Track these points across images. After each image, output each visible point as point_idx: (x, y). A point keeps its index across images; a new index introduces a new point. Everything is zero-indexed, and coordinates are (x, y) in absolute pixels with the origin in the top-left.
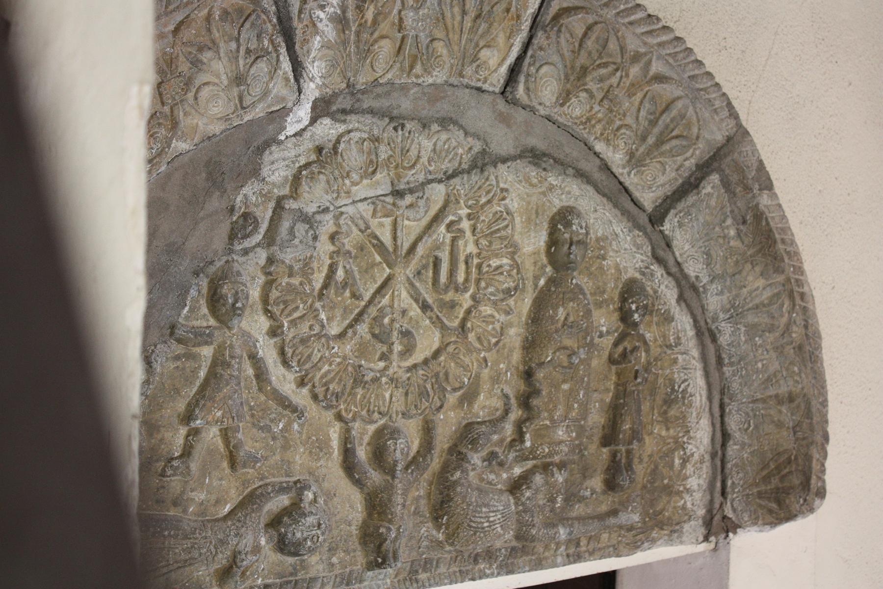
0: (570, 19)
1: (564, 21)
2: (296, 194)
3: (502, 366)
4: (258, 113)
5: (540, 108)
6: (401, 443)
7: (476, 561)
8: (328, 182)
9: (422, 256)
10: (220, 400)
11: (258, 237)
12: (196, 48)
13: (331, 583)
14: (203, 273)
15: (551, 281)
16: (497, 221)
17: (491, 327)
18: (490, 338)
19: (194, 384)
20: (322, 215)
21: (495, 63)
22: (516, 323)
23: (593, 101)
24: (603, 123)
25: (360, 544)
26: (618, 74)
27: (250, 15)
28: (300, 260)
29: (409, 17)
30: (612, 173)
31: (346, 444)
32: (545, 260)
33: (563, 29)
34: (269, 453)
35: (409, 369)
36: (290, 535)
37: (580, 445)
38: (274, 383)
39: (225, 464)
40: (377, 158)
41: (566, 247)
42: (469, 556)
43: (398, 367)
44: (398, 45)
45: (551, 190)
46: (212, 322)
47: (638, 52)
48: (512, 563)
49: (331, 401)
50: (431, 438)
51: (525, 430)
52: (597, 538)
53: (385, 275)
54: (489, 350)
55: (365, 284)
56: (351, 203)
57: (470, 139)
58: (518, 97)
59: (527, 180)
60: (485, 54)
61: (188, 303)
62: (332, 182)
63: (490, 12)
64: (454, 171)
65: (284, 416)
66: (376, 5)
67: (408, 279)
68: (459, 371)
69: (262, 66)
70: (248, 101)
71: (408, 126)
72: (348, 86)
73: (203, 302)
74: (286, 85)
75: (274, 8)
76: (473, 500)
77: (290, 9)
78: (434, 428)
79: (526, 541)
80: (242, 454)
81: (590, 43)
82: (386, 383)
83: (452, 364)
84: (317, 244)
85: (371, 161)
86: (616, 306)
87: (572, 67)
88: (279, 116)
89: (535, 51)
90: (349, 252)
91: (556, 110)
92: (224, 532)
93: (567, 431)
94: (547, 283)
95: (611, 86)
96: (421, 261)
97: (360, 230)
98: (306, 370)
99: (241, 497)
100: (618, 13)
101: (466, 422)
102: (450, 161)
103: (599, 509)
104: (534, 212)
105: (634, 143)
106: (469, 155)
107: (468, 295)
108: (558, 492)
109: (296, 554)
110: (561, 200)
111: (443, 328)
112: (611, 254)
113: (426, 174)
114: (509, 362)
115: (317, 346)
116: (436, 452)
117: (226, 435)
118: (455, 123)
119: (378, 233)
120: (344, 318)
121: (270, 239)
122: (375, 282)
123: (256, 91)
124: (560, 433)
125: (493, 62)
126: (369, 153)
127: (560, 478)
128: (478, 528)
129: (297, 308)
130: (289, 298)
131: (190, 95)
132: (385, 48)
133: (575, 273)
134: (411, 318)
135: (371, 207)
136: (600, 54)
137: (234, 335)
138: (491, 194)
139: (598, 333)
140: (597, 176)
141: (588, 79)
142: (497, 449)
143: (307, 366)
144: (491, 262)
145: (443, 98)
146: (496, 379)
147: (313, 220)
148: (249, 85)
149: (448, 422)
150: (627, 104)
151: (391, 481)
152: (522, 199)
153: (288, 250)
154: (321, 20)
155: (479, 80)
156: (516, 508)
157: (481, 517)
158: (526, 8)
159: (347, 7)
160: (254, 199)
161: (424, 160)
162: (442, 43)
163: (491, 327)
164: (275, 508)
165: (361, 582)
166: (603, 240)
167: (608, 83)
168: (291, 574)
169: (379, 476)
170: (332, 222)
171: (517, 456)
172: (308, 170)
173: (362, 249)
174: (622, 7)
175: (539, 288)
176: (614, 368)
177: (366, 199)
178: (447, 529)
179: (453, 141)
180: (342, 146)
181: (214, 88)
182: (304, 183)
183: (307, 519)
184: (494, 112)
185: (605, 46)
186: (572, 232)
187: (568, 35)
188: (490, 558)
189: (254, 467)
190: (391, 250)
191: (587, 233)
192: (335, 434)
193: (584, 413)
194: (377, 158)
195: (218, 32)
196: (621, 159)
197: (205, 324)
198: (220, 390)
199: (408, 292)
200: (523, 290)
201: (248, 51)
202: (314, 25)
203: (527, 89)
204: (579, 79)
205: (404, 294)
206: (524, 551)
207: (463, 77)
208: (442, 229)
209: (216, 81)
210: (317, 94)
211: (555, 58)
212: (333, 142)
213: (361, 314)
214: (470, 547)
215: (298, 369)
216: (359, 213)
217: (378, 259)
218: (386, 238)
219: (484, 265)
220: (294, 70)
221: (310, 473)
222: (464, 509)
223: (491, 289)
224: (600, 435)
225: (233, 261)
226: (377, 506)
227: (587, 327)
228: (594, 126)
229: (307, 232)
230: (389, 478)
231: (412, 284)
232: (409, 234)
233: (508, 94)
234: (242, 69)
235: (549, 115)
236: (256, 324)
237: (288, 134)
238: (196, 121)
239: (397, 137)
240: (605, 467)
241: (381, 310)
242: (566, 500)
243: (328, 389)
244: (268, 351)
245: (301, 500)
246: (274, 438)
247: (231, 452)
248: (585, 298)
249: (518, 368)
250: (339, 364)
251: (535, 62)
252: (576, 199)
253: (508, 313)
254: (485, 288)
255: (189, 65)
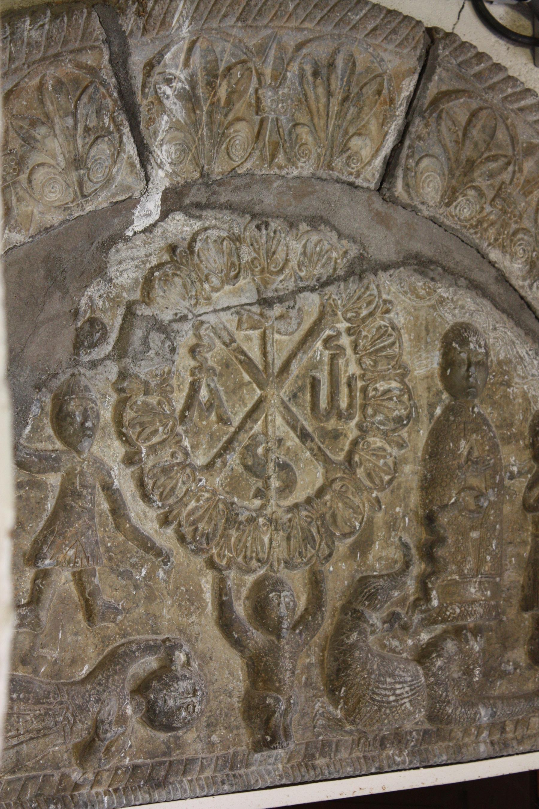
0: (451, 104)
1: (444, 106)
2: (149, 298)
3: (398, 509)
4: (100, 203)
5: (423, 208)
6: (285, 596)
7: (383, 746)
8: (184, 286)
9: (297, 376)
10: (72, 536)
11: (107, 348)
12: (27, 121)
13: (212, 766)
14: (46, 387)
15: (448, 410)
16: (381, 337)
17: (382, 461)
18: (383, 475)
19: (41, 518)
20: (180, 324)
21: (369, 154)
22: (411, 459)
23: (483, 200)
24: (497, 226)
25: (244, 719)
26: (510, 169)
27: (87, 87)
28: (157, 375)
29: (268, 97)
30: (511, 285)
31: (221, 596)
32: (440, 385)
33: (444, 115)
34: (130, 605)
35: (290, 509)
36: (160, 703)
37: (497, 606)
38: (133, 520)
39: (80, 616)
40: (239, 260)
41: (465, 368)
42: (375, 739)
43: (277, 506)
44: (256, 130)
45: (441, 303)
46: (58, 445)
47: (531, 143)
48: (426, 750)
49: (201, 544)
50: (321, 592)
51: (430, 586)
52: (526, 723)
53: (256, 398)
54: (382, 489)
55: (233, 407)
56: (212, 311)
57: (344, 242)
58: (396, 194)
59: (414, 291)
60: (355, 143)
61: (29, 421)
62: (189, 286)
63: (359, 94)
64: (329, 277)
65: (146, 561)
66: (229, 82)
67: (283, 402)
68: (348, 513)
69: (103, 149)
70: (89, 188)
71: (273, 225)
72: (202, 175)
73: (47, 421)
74: (132, 172)
75: (114, 80)
76: (375, 667)
77: (133, 82)
78: (322, 581)
79: (441, 723)
80: (99, 603)
81: (475, 133)
82: (264, 525)
83: (340, 505)
84: (176, 357)
85: (233, 264)
86: (527, 442)
87: (457, 160)
88: (125, 207)
89: (412, 141)
90: (213, 369)
91: (441, 211)
92: (83, 697)
93: (480, 588)
94: (444, 412)
95: (503, 183)
96: (296, 382)
97: (224, 343)
98: (170, 506)
99: (101, 657)
100: (506, 98)
101: (360, 575)
102: (323, 266)
103: (525, 688)
104: (423, 328)
105: (534, 250)
106: (345, 260)
107: (353, 423)
108: (475, 662)
109: (168, 728)
110: (454, 315)
111: (327, 461)
112: (516, 380)
113: (296, 281)
114: (406, 506)
115: (181, 477)
116: (328, 610)
117: (80, 579)
118: (327, 223)
119: (245, 348)
120: (211, 447)
121: (121, 351)
122: (245, 405)
123: (98, 176)
124: (473, 590)
125: (366, 153)
126: (230, 254)
127: (476, 646)
128: (383, 702)
129: (156, 431)
130: (146, 419)
131: (23, 177)
132: (242, 133)
133: (476, 401)
134: (289, 448)
135: (236, 318)
136: (488, 145)
137: (84, 460)
138: (373, 306)
139: (508, 474)
140: (494, 288)
141: (476, 174)
142: (399, 610)
143: (171, 501)
144: (378, 385)
145: (312, 193)
146: (392, 525)
147: (169, 329)
148: (89, 169)
149: (339, 575)
150: (523, 204)
151: (276, 642)
152: (409, 313)
153: (143, 363)
154: (168, 97)
155: (351, 174)
156: (426, 680)
157: (385, 689)
158: (400, 91)
159: (197, 83)
160: (101, 303)
161: (293, 263)
162: (306, 129)
163: (382, 461)
164: (140, 671)
165: (248, 765)
166: (506, 364)
167: (499, 179)
168: (164, 754)
169: (261, 636)
170: (191, 333)
171: (422, 619)
172: (161, 272)
173: (227, 365)
174: (510, 91)
175: (435, 418)
176: (530, 516)
177: (228, 308)
178: (345, 703)
179: (326, 243)
180: (198, 246)
181: (50, 170)
182: (157, 286)
183: (180, 683)
184: (370, 211)
185: (492, 136)
186: (470, 351)
187: (450, 123)
188: (400, 742)
189: (114, 621)
190: (261, 367)
191: (487, 354)
192: (207, 584)
193: (499, 568)
194: (239, 260)
195: (53, 105)
196: (521, 270)
197: (50, 447)
198: (71, 525)
199: (284, 418)
200: (417, 420)
201: (87, 129)
202: (161, 102)
203: (407, 186)
204: (465, 174)
205: (279, 421)
206: (440, 735)
207: (332, 169)
208: (319, 345)
209: (52, 162)
210: (167, 183)
211: (437, 150)
212: (188, 241)
213: (230, 441)
214: (375, 727)
215: (160, 504)
216: (222, 323)
217: (247, 378)
218: (255, 353)
219: (370, 389)
220: (140, 154)
221: (181, 631)
222: (364, 678)
223: (379, 418)
224: (520, 597)
225: (80, 374)
226: (261, 672)
227: (495, 464)
228: (486, 230)
229: (163, 343)
230: (274, 638)
231: (287, 408)
232: (280, 350)
233: (384, 191)
234: (80, 150)
235: (434, 217)
236: (109, 451)
237: (137, 229)
238: (30, 208)
239: (261, 236)
240: (529, 636)
241: (253, 438)
242: (485, 675)
243: (196, 529)
244: (124, 482)
245: (172, 661)
246: (136, 587)
247: (86, 601)
248: (490, 430)
249: (417, 512)
250: (208, 500)
251: (413, 152)
252: (471, 315)
253: (401, 446)
254: (374, 415)
255: (20, 141)
